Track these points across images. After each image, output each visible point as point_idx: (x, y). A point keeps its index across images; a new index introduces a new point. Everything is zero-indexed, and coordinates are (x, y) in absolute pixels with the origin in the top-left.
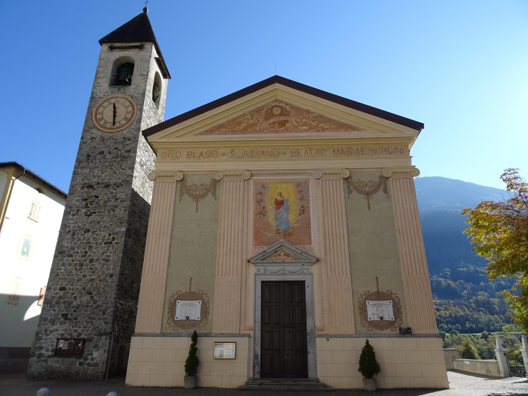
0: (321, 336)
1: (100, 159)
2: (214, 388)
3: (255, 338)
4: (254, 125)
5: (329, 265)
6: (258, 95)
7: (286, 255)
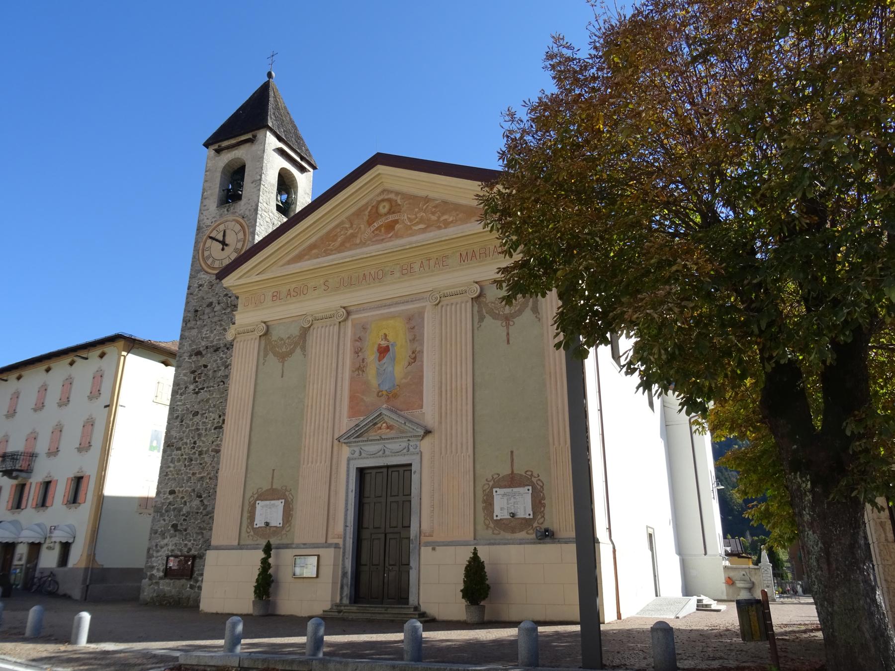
0: (427, 544)
1: (208, 314)
2: (292, 616)
3: (344, 549)
4: (353, 236)
5: (443, 438)
6: (354, 190)
7: (388, 427)
